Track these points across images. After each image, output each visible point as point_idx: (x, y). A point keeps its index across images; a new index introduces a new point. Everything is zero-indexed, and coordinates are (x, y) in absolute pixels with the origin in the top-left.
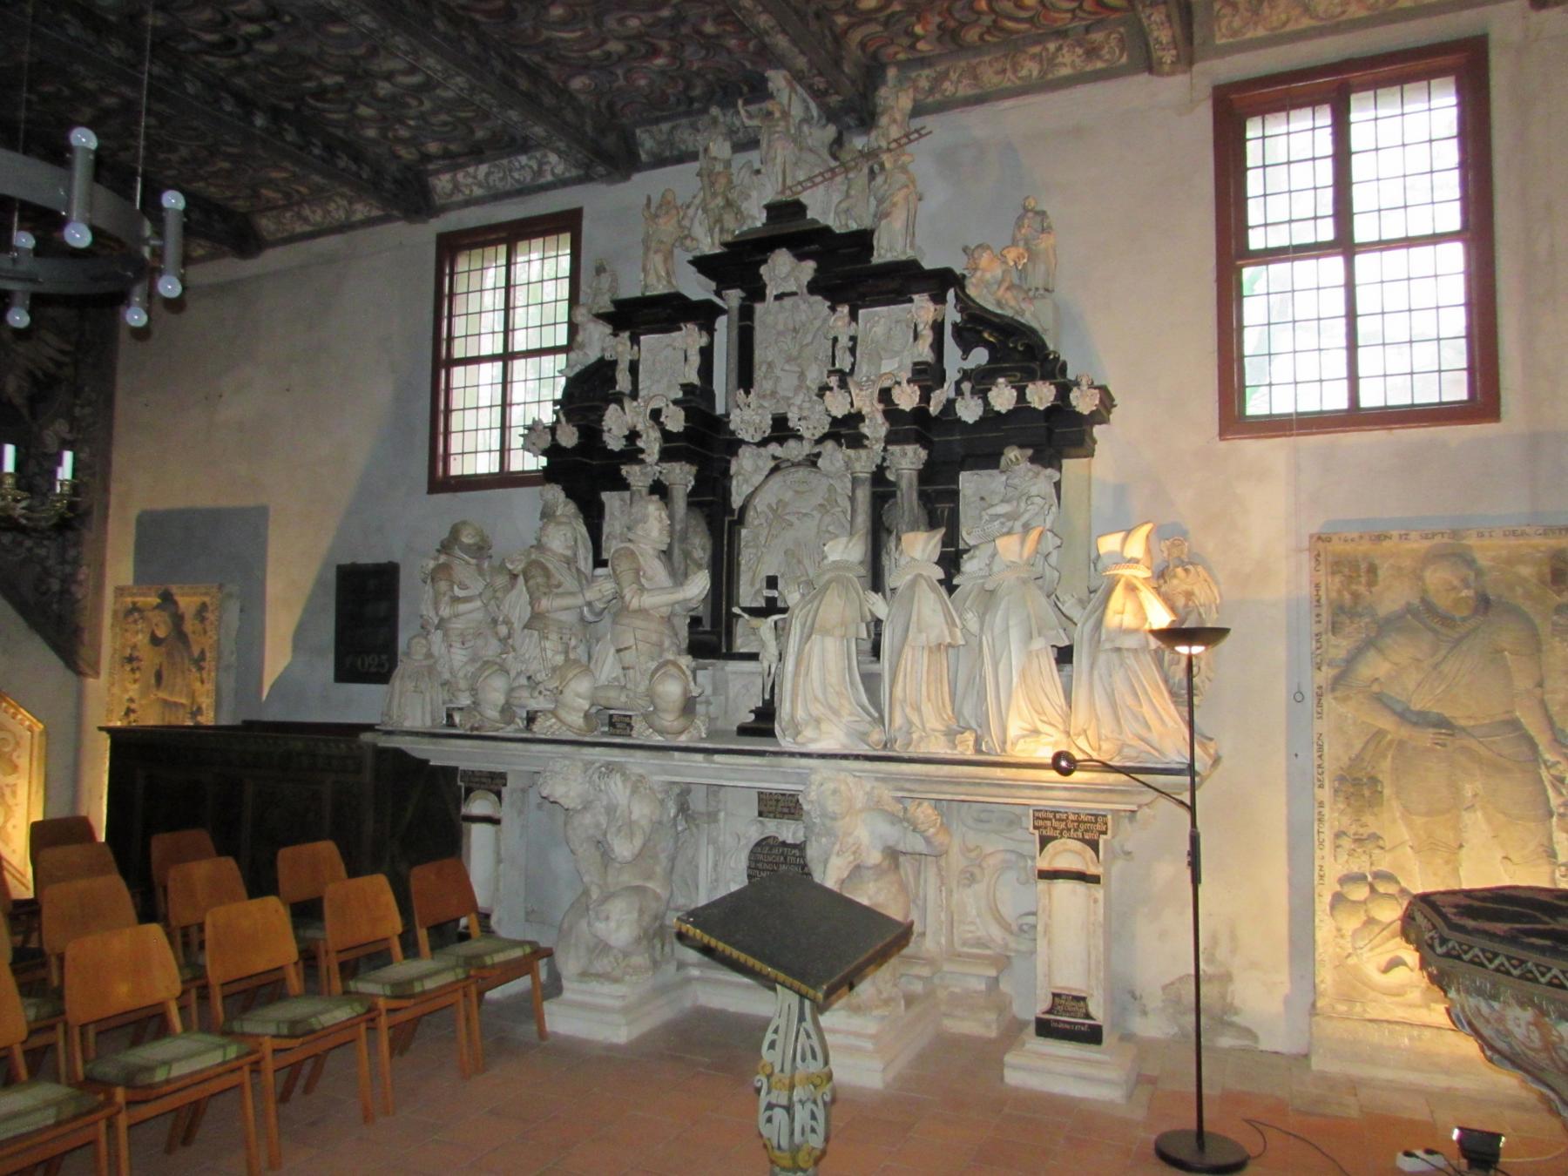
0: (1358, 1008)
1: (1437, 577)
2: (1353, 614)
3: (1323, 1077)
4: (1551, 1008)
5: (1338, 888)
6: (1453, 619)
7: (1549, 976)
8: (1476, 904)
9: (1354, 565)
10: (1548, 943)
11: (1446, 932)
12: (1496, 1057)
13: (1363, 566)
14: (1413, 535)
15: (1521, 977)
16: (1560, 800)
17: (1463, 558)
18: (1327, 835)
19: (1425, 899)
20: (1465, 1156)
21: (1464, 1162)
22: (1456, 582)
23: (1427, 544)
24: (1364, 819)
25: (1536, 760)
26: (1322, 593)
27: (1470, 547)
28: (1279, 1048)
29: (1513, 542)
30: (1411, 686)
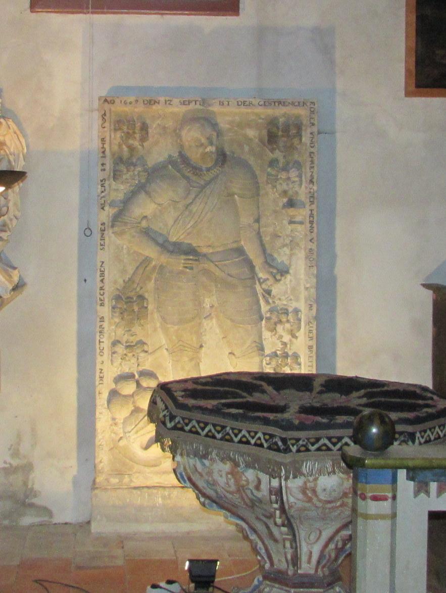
0: (126, 479)
1: (192, 135)
2: (129, 164)
3: (104, 541)
4: (241, 460)
5: (113, 386)
6: (201, 170)
7: (240, 436)
8: (200, 387)
9: (131, 123)
10: (241, 411)
11: (175, 411)
12: (207, 501)
13: (138, 125)
14: (176, 101)
15: (222, 439)
16: (268, 308)
17: (207, 120)
18: (106, 344)
19: (165, 388)
20: (193, 581)
21: (192, 585)
22: (203, 140)
23: (184, 109)
24: (133, 329)
25: (253, 278)
26: (107, 146)
27: (213, 113)
28: (68, 520)
29: (244, 110)
30: (171, 222)
